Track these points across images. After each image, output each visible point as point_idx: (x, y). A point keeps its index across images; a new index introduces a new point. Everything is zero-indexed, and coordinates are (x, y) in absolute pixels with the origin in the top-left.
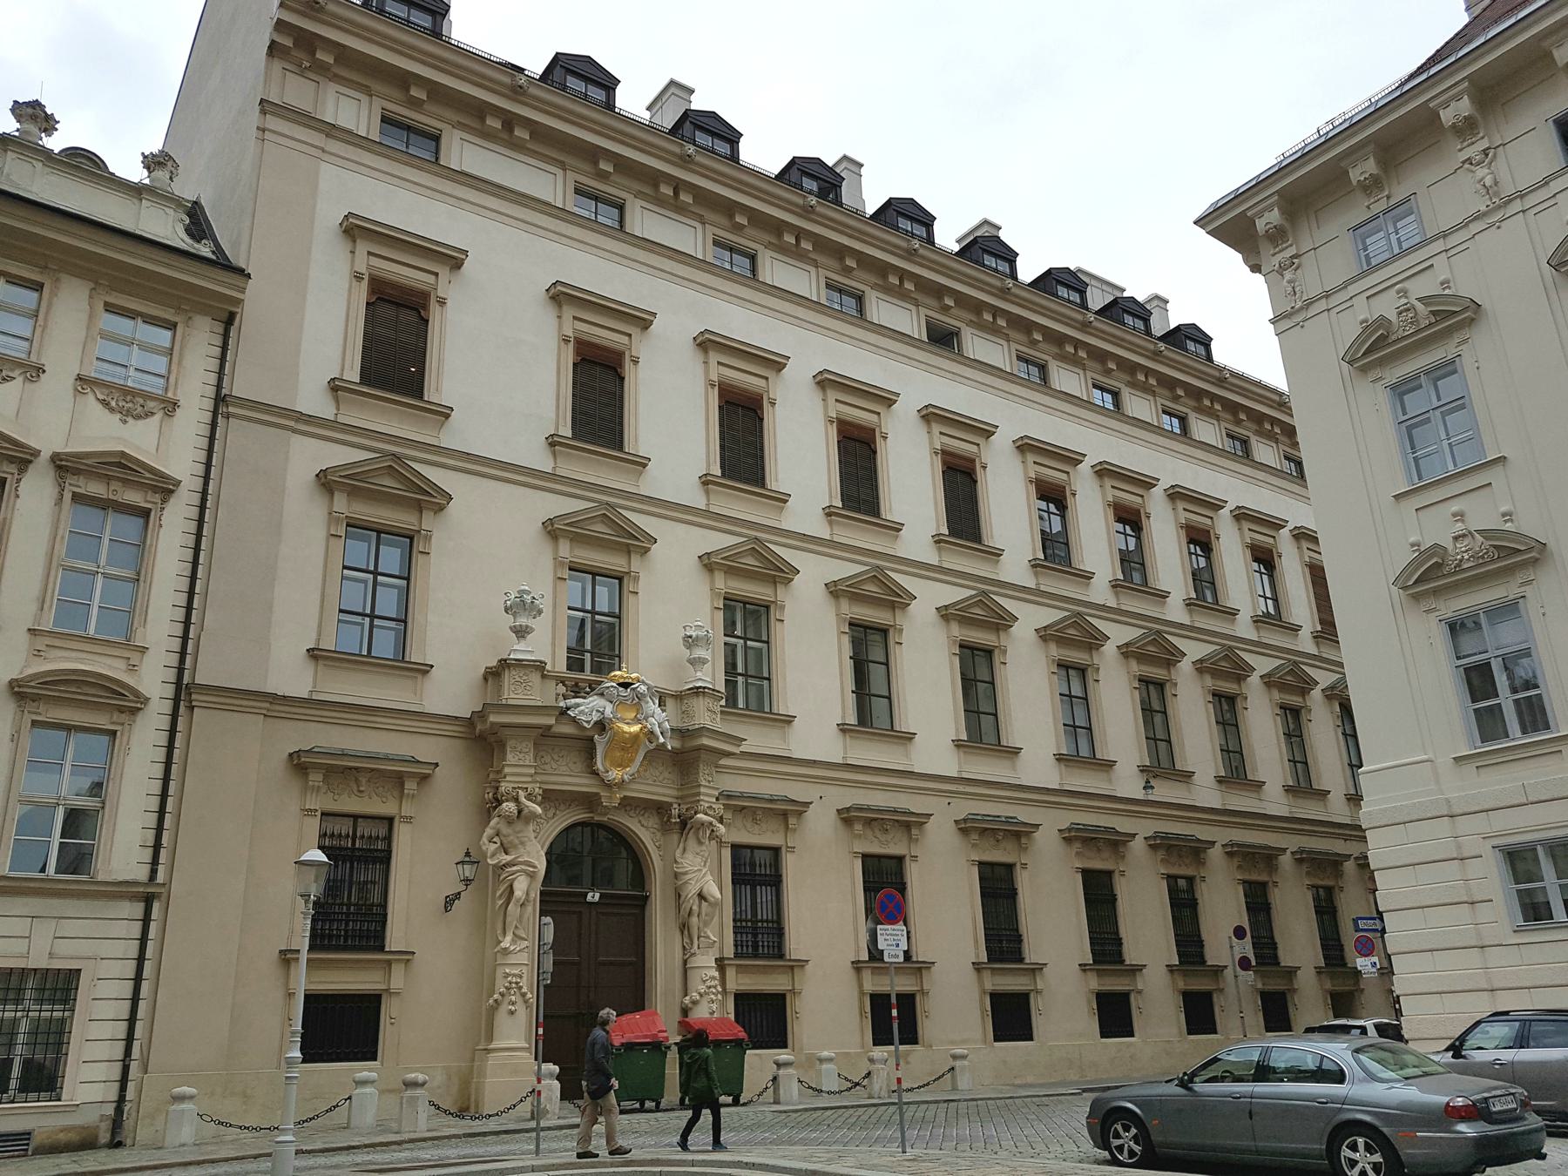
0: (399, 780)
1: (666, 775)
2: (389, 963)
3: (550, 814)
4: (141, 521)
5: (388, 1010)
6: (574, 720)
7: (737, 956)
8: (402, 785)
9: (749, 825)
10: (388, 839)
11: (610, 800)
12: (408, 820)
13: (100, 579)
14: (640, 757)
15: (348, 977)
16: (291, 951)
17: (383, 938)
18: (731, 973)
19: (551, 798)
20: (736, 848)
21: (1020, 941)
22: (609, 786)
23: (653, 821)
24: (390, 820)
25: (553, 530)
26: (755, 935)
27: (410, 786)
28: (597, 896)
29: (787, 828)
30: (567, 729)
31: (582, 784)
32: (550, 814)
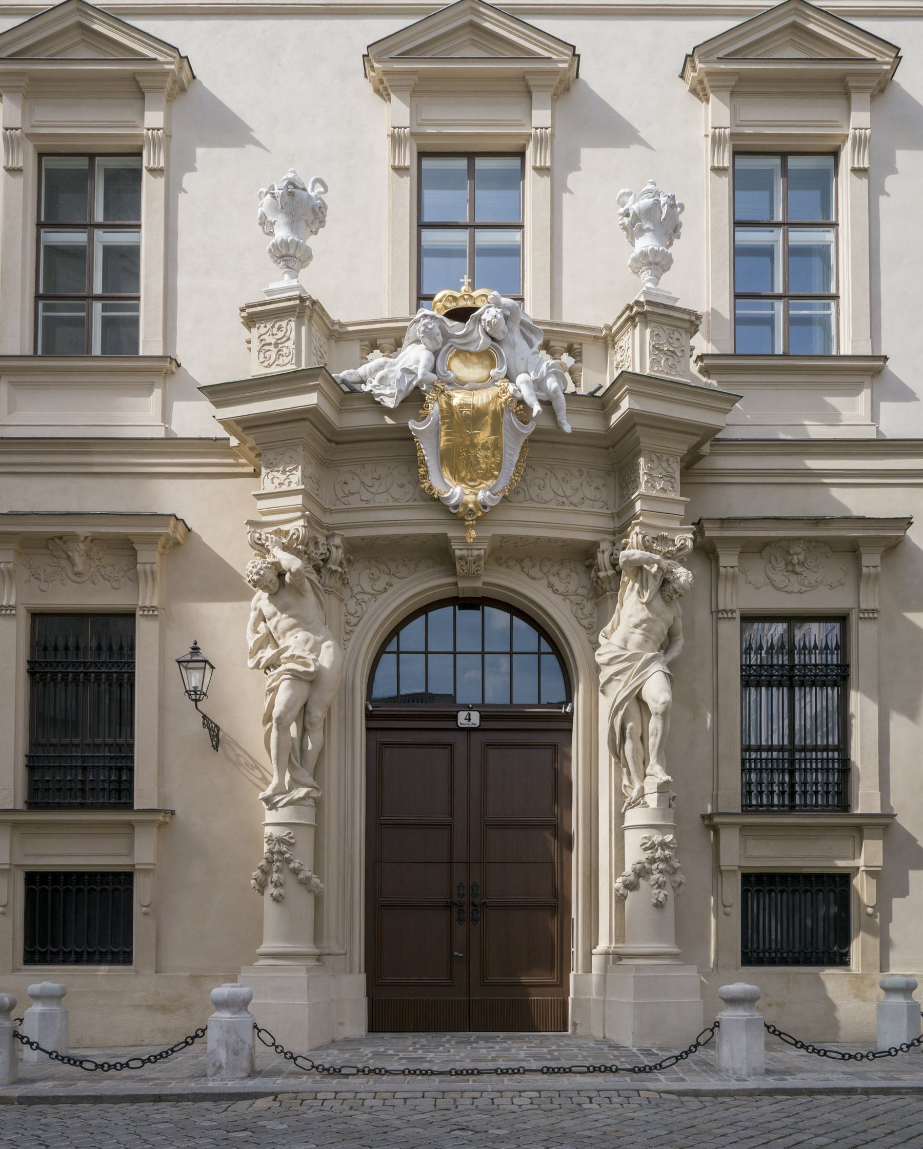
0: (126, 547)
1: (589, 492)
2: (130, 825)
3: (380, 585)
4: (816, 194)
5: (143, 892)
6: (370, 396)
7: (747, 808)
8: (134, 554)
9: (779, 577)
10: (843, 646)
11: (470, 541)
12: (871, 615)
13: (779, 289)
14: (512, 455)
15: (76, 846)
16: (165, 812)
17: (130, 791)
18: (730, 840)
19: (370, 552)
20: (748, 619)
21: (29, 757)
22: (457, 515)
23: (574, 581)
24: (842, 619)
25: (375, 52)
26: (792, 773)
27: (870, 560)
28: (475, 718)
29: (859, 574)
30: (363, 420)
31: (416, 523)
32: (380, 585)
